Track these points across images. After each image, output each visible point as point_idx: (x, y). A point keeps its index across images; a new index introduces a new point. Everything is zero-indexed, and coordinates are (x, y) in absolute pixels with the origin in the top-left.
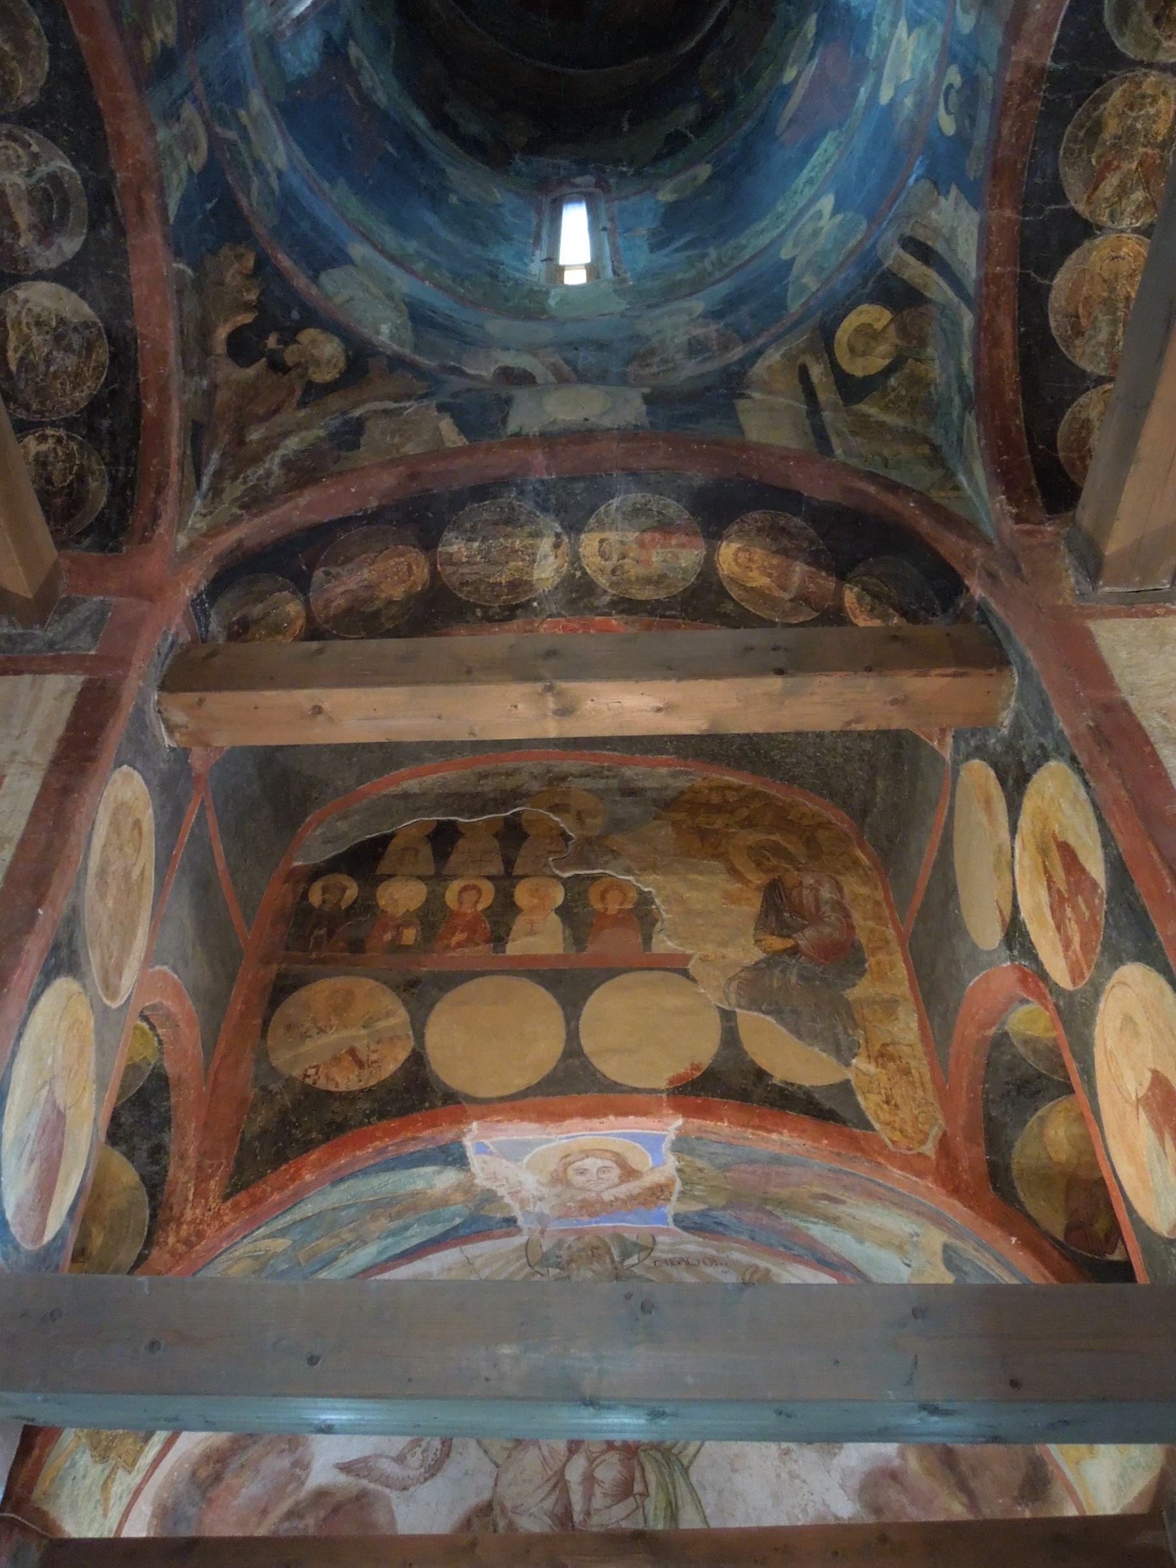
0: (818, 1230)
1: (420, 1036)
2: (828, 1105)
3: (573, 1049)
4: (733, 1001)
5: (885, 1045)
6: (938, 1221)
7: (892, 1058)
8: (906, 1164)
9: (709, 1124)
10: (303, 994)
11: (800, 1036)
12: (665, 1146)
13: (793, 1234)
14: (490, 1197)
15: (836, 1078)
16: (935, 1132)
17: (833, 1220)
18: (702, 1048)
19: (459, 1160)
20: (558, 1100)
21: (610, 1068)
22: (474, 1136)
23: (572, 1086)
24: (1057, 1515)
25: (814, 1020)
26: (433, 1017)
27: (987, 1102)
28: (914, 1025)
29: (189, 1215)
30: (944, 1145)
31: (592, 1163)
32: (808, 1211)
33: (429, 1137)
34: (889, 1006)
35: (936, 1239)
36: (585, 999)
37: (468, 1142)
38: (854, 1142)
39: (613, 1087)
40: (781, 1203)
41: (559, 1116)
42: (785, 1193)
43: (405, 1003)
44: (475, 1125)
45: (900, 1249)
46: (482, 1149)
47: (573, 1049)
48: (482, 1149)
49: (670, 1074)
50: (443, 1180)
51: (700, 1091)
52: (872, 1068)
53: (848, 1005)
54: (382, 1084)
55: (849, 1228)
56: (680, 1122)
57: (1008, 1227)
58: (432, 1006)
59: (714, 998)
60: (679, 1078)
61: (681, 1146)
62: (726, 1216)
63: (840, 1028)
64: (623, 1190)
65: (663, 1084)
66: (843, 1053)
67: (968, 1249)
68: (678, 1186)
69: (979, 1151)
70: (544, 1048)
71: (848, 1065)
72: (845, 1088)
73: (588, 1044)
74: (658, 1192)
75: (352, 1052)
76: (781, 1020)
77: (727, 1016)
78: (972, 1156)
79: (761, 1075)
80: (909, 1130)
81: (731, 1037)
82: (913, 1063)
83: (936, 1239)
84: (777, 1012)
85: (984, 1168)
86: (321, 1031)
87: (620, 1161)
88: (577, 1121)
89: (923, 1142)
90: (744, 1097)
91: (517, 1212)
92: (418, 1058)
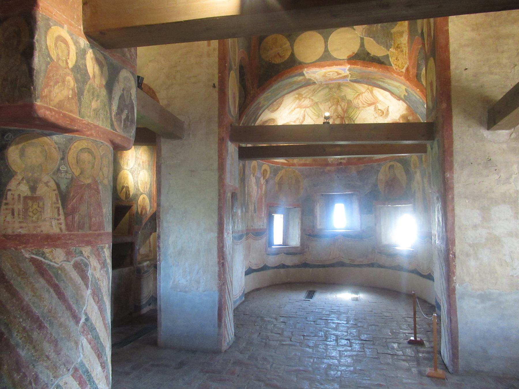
0: (380, 83)
1: (293, 49)
2: (382, 60)
3: (326, 50)
4: (364, 35)
5: (398, 45)
6: (404, 84)
7: (399, 48)
8: (398, 74)
9: (356, 66)
10: (266, 40)
11: (378, 44)
12: (346, 70)
13: (375, 83)
14: (310, 80)
15: (386, 54)
16: (406, 66)
17: (384, 82)
18: (355, 48)
19: (303, 75)
20: (323, 63)
21: (334, 54)
22: (305, 71)
23: (326, 59)
24: (453, 113)
25: (382, 39)
26: (295, 44)
27: (418, 60)
28: (407, 39)
29: (251, 93)
30: (407, 69)
31: (331, 73)
32: (378, 80)
33: (296, 72)
34: (401, 34)
35: (404, 87)
36: (329, 36)
37: (304, 72)
38: (387, 69)
39: (335, 59)
40: (372, 79)
41: (323, 66)
42: (373, 77)
43: (288, 40)
44: (306, 69)
45: (397, 87)
46: (307, 73)
47: (326, 50)
48: (307, 73)
49: (347, 55)
50: (301, 78)
51: (354, 59)
52: (394, 51)
53: (391, 34)
54: (285, 61)
55: (386, 83)
56: (349, 66)
57: (417, 87)
58: (295, 41)
59: (359, 35)
60: (350, 56)
61: (350, 70)
62: (361, 80)
63: (388, 41)
64: (338, 76)
65: (346, 58)
66: (388, 47)
67: (410, 90)
68: (350, 76)
69: (415, 71)
70: (320, 50)
71: (389, 50)
72: (387, 56)
73: (329, 49)
74: (346, 77)
75: (278, 54)
76: (374, 39)
77: (362, 39)
78: (413, 72)
79: (368, 54)
80: (400, 66)
81: (362, 45)
82: (404, 49)
83: (404, 87)
84: (374, 38)
85: (415, 74)
86: (271, 49)
87: (337, 72)
88: (327, 67)
89: (403, 69)
90: (364, 59)
91: (315, 81)
92: (293, 54)
